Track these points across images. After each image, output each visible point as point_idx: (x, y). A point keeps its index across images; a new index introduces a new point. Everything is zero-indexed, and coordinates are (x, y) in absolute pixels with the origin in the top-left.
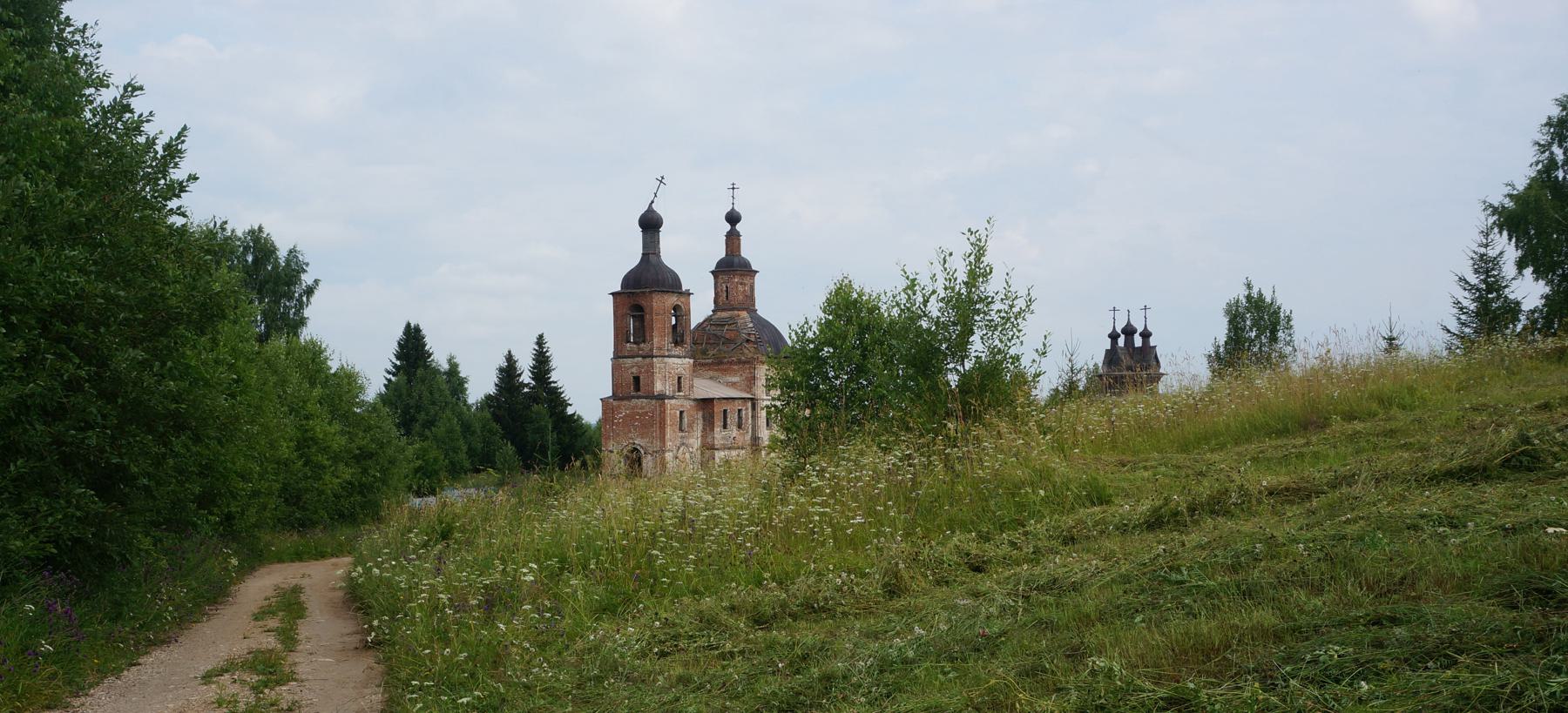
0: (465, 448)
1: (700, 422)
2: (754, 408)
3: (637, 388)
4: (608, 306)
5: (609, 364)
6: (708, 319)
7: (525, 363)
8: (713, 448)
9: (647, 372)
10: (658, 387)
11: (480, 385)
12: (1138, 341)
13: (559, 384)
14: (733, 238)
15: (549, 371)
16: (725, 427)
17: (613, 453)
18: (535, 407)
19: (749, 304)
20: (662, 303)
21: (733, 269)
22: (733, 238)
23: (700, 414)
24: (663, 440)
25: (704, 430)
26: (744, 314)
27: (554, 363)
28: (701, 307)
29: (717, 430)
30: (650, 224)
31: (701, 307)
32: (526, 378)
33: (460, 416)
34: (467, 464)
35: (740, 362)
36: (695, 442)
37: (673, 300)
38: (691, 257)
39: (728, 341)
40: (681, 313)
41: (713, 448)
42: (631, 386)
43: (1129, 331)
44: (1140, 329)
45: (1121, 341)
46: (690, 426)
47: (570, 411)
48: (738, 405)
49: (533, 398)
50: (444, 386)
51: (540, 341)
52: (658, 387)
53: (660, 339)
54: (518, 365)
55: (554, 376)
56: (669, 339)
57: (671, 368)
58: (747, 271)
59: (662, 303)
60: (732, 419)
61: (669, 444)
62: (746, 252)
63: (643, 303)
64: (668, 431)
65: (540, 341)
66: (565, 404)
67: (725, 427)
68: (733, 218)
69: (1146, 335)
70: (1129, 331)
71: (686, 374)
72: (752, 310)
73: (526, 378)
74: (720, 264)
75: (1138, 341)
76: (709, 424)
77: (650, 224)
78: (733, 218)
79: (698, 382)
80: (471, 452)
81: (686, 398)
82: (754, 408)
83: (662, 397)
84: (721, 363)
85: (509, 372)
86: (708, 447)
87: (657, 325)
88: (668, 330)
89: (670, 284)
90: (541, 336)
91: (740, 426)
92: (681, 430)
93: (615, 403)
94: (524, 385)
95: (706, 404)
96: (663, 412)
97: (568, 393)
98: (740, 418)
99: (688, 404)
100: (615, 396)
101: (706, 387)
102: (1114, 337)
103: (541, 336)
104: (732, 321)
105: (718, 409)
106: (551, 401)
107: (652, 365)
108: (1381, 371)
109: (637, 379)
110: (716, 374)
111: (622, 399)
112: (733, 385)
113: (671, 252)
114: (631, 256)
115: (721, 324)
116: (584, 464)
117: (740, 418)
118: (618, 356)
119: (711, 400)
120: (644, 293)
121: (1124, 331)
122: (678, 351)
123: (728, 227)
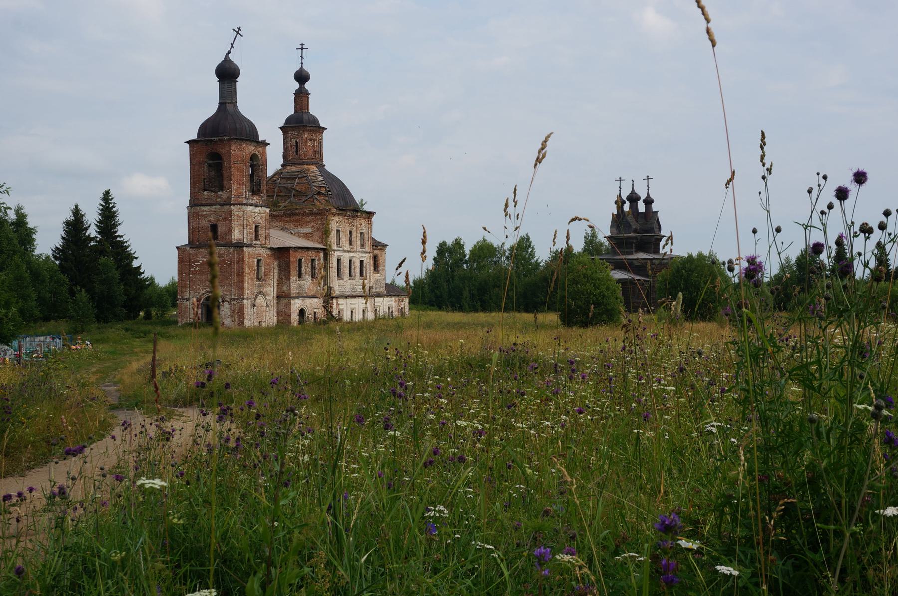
0: (34, 296)
1: (276, 271)
2: (326, 258)
3: (215, 236)
4: (184, 154)
5: (185, 213)
6: (278, 173)
7: (92, 217)
8: (288, 297)
9: (226, 219)
10: (237, 235)
11: (47, 241)
12: (641, 207)
13: (125, 238)
14: (301, 97)
15: (115, 225)
16: (300, 275)
17: (190, 305)
18: (103, 259)
19: (317, 159)
20: (241, 151)
21: (301, 125)
22: (301, 97)
23: (276, 264)
24: (241, 289)
25: (280, 280)
26: (313, 168)
27: (120, 218)
28: (274, 161)
29: (293, 278)
30: (227, 74)
31: (274, 161)
32: (93, 232)
33: (29, 263)
34: (37, 313)
35: (312, 213)
36: (272, 290)
37: (250, 149)
38: (265, 108)
39: (299, 194)
40: (257, 163)
41: (288, 297)
42: (207, 239)
43: (633, 198)
44: (643, 196)
45: (626, 207)
46: (267, 274)
47: (135, 264)
48: (311, 255)
49: (100, 250)
50: (12, 235)
51: (107, 197)
52: (237, 235)
53: (238, 187)
54: (86, 218)
55: (120, 230)
56: (246, 187)
57: (249, 216)
58: (316, 128)
59: (241, 151)
60: (307, 269)
61: (247, 292)
62: (314, 109)
63: (221, 151)
64: (247, 278)
65: (107, 197)
66: (130, 257)
67: (300, 275)
68: (302, 77)
69: (648, 202)
70: (633, 198)
71: (263, 223)
72: (321, 166)
73: (93, 232)
74: (289, 120)
75: (641, 207)
76: (285, 274)
77: (227, 74)
78: (302, 77)
79: (273, 232)
80: (40, 300)
81: (263, 246)
82: (326, 258)
83: (240, 245)
84: (293, 214)
85: (75, 225)
86: (283, 297)
87: (235, 173)
88: (246, 179)
89: (248, 133)
90: (107, 193)
91: (313, 276)
92: (258, 278)
93: (192, 251)
94: (90, 239)
95: (282, 253)
96: (241, 260)
97: (134, 247)
98: (313, 267)
99: (265, 253)
100: (191, 244)
101: (281, 238)
102: (620, 203)
103: (107, 193)
104: (303, 175)
105: (294, 257)
106: (118, 254)
107: (230, 213)
108: (538, 312)
109: (214, 227)
110: (287, 225)
111: (199, 247)
112: (305, 235)
113: (248, 103)
114: (210, 108)
115: (292, 177)
116: (148, 317)
117: (313, 267)
118: (194, 203)
119: (287, 249)
120: (219, 145)
121: (629, 198)
122: (255, 200)
123: (297, 85)
